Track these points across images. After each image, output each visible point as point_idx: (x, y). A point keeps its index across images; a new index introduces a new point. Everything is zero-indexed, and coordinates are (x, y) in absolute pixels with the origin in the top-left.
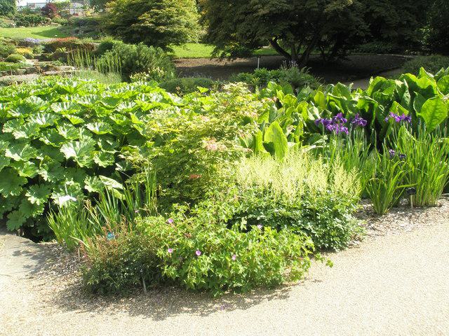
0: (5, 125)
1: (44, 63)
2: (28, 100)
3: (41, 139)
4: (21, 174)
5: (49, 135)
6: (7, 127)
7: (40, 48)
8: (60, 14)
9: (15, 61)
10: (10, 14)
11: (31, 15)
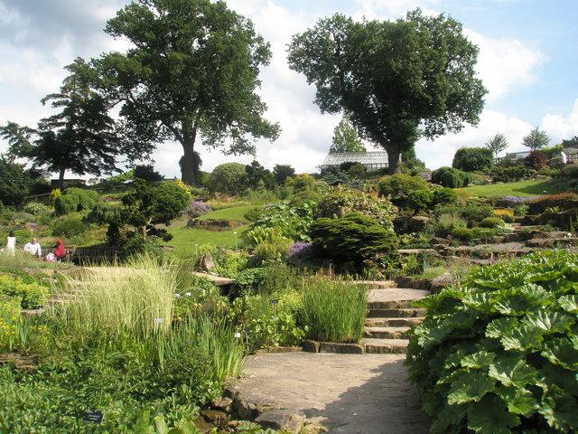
0: (489, 326)
1: (529, 229)
2: (524, 290)
3: (544, 354)
4: (511, 408)
5: (557, 347)
6: (492, 329)
7: (523, 208)
8: (548, 164)
9: (491, 225)
10: (486, 168)
11: (511, 168)
